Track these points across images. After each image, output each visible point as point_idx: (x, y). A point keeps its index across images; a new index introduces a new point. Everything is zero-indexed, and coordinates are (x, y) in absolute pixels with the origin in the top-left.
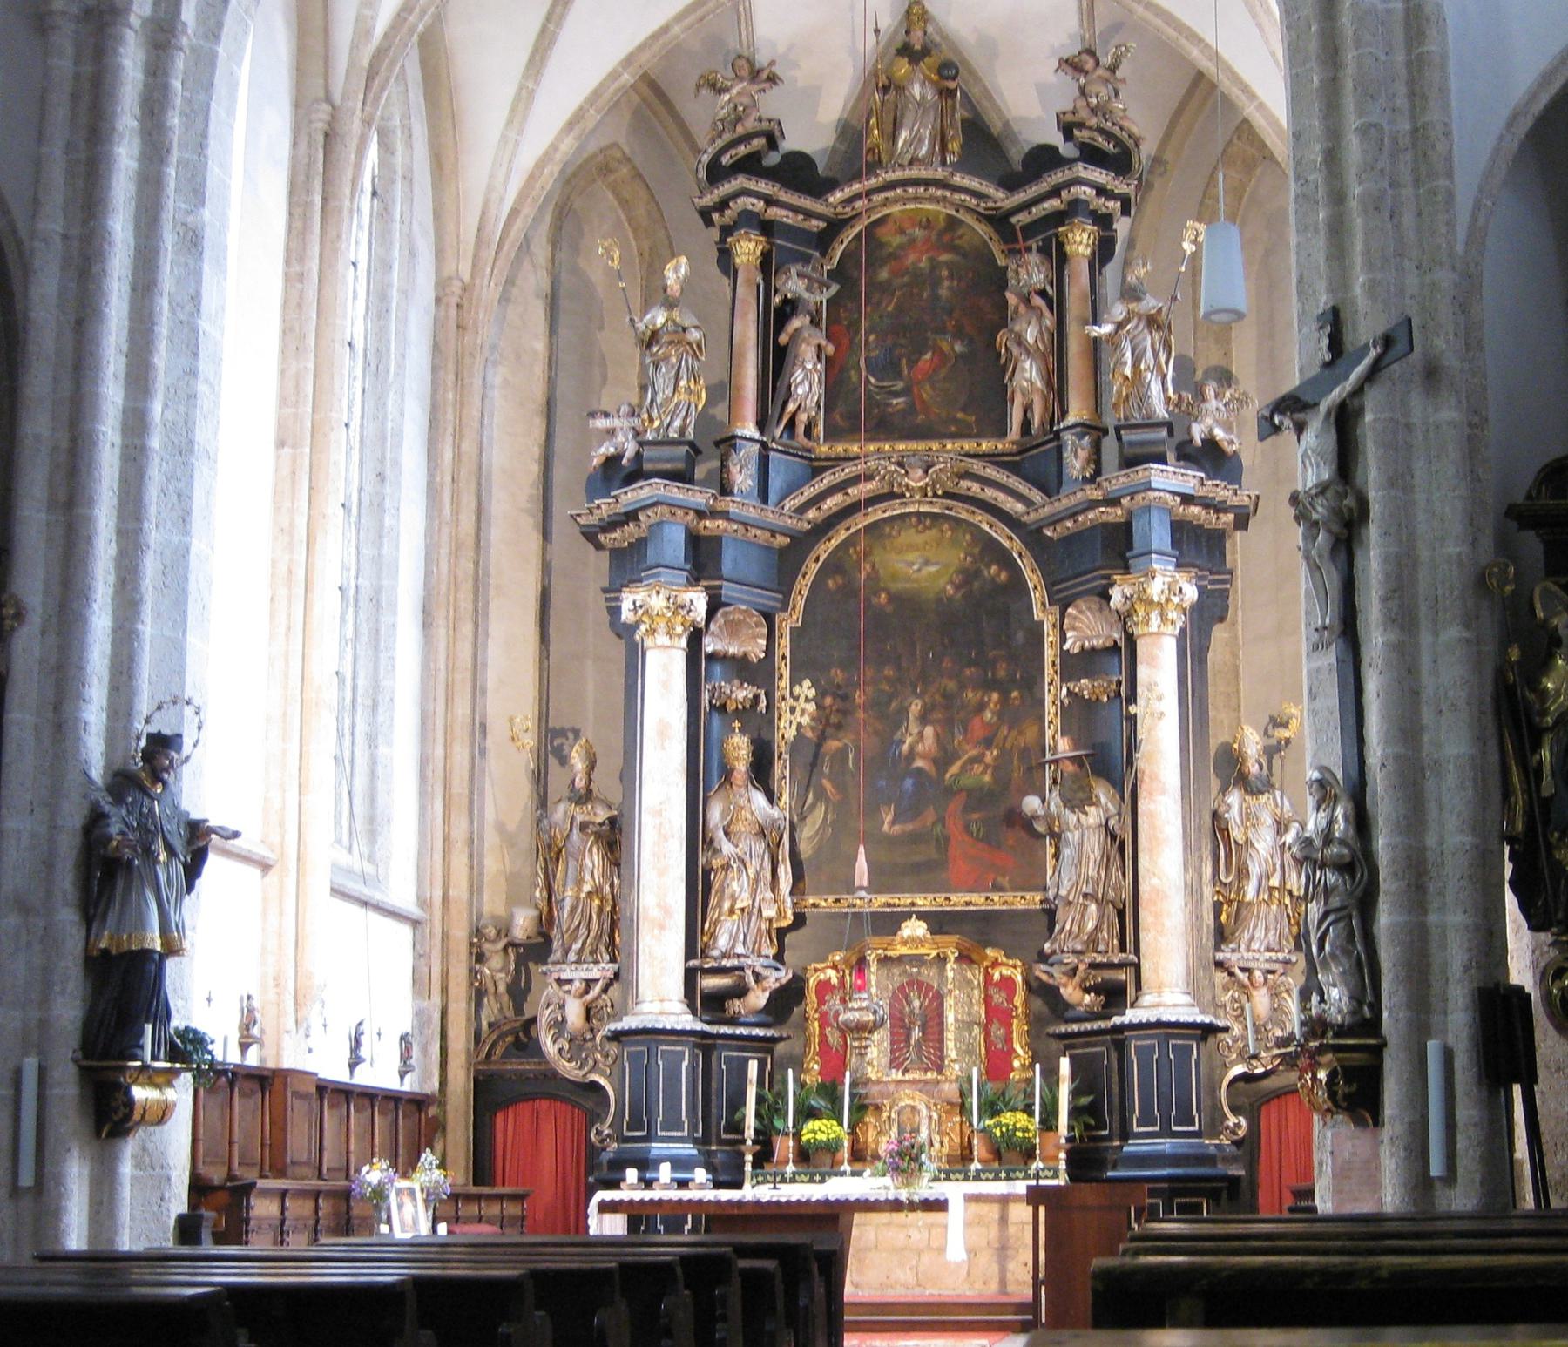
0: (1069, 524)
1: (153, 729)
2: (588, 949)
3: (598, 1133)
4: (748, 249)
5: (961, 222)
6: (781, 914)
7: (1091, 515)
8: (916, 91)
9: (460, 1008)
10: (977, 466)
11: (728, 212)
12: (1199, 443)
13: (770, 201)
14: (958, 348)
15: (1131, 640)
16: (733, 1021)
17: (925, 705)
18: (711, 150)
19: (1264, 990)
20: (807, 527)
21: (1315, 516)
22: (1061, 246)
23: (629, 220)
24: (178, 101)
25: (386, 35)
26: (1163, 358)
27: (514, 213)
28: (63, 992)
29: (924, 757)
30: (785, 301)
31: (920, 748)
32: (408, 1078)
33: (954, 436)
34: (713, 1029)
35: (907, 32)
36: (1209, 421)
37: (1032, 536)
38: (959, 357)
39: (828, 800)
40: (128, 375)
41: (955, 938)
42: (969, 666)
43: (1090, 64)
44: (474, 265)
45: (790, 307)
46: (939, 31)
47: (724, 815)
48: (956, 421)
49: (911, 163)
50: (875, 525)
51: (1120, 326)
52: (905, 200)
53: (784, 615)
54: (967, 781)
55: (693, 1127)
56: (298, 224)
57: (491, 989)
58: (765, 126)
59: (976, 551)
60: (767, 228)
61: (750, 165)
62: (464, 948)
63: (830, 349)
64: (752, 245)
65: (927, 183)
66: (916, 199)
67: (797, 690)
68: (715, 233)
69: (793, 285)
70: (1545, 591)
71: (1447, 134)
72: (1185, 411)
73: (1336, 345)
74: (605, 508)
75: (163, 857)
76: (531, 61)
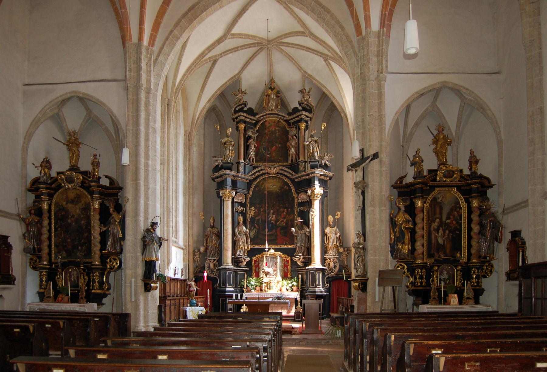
0: (300, 179)
2: (214, 254)
3: (216, 286)
4: (242, 126)
6: (248, 248)
7: (304, 177)
8: (272, 96)
11: (238, 119)
12: (324, 164)
13: (246, 117)
14: (280, 146)
15: (311, 201)
16: (240, 267)
17: (273, 212)
19: (333, 262)
21: (359, 187)
22: (299, 127)
24: (151, 104)
26: (317, 148)
27: (198, 118)
29: (273, 220)
30: (248, 136)
31: (272, 219)
33: (279, 162)
34: (236, 268)
35: (271, 85)
37: (293, 181)
44: (191, 128)
47: (238, 230)
48: (279, 159)
50: (264, 179)
51: (310, 142)
53: (248, 195)
54: (281, 225)
55: (233, 286)
58: (244, 102)
59: (283, 183)
60: (245, 122)
61: (241, 110)
63: (257, 145)
64: (242, 126)
65: (274, 114)
67: (251, 208)
68: (235, 123)
69: (250, 134)
72: (322, 158)
73: (363, 155)
74: (216, 175)
75: (155, 244)
76: (201, 89)
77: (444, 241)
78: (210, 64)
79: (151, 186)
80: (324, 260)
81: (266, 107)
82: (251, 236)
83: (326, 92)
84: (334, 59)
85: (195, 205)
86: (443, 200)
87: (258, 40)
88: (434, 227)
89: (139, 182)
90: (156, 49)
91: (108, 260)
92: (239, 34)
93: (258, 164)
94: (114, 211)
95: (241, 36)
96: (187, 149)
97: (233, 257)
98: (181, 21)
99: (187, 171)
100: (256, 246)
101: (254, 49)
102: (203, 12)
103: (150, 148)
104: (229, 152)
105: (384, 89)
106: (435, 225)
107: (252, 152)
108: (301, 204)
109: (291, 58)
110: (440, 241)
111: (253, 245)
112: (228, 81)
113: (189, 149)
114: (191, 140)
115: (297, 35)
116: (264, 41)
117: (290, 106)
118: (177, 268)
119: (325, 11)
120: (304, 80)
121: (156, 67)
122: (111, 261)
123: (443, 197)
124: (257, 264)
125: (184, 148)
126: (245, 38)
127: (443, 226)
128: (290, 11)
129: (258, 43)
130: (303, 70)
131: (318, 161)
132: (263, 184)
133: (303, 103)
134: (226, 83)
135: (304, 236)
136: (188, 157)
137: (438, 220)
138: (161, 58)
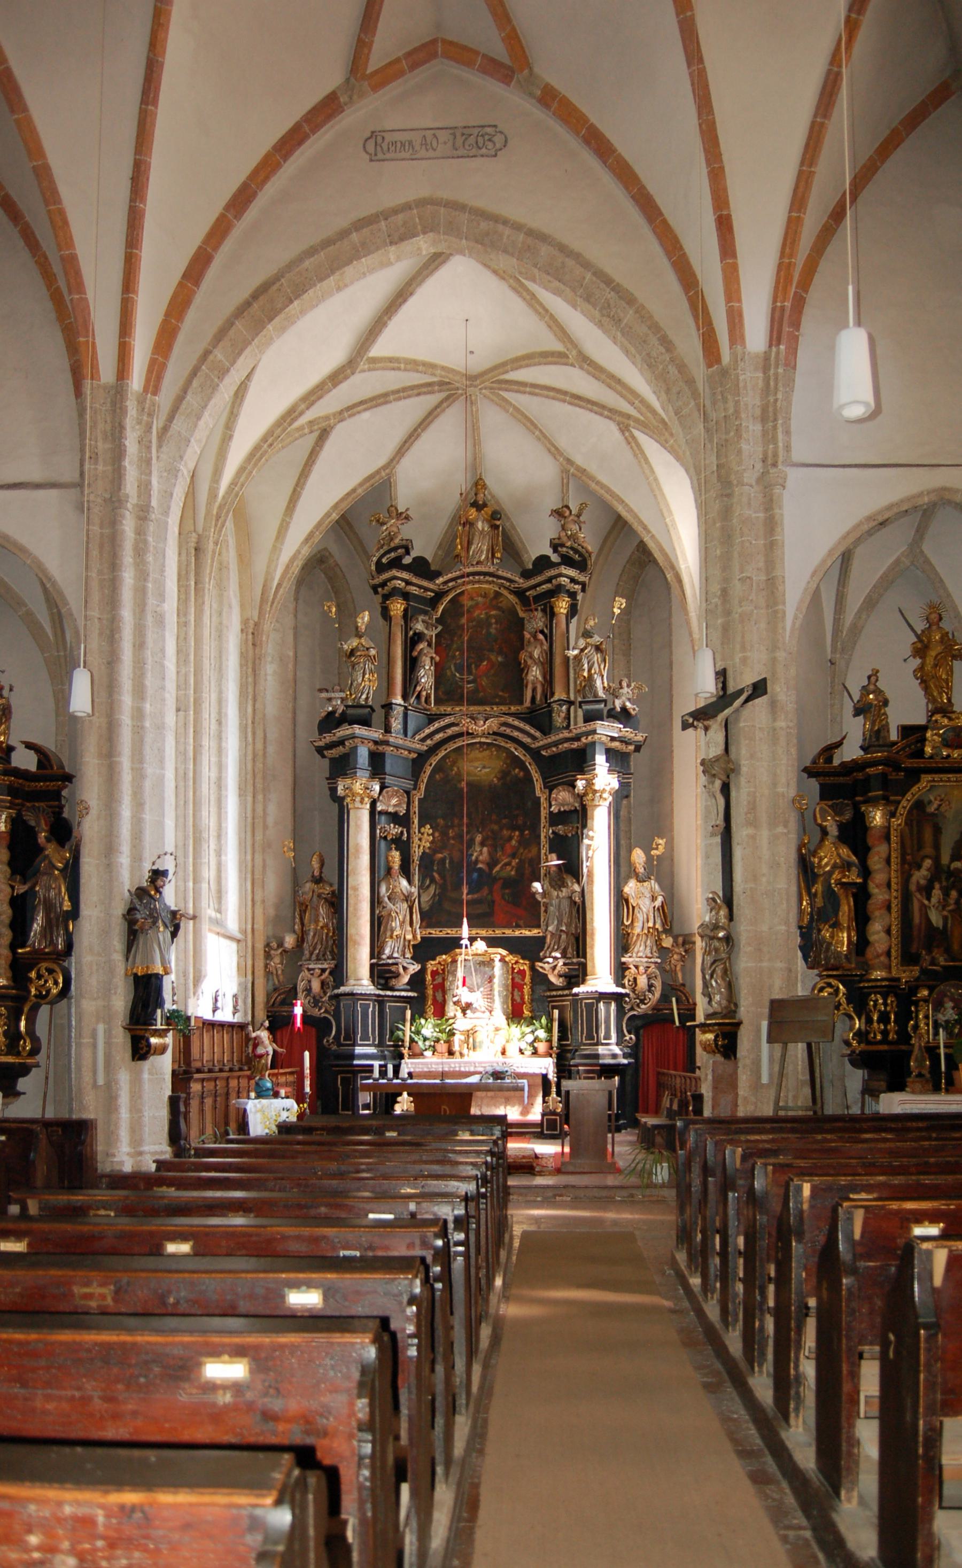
0: (554, 749)
1: (155, 868)
3: (328, 1041)
4: (397, 607)
5: (502, 594)
9: (260, 982)
10: (510, 720)
12: (619, 709)
13: (408, 583)
14: (500, 659)
18: (378, 555)
19: (645, 976)
20: (426, 748)
21: (714, 772)
22: (552, 608)
23: (332, 588)
25: (224, 497)
26: (602, 667)
28: (115, 993)
29: (482, 862)
30: (415, 634)
32: (236, 1015)
33: (497, 704)
35: (476, 494)
36: (624, 698)
37: (535, 754)
38: (501, 663)
39: (436, 883)
40: (134, 690)
41: (501, 951)
42: (505, 818)
43: (567, 513)
45: (418, 637)
46: (490, 493)
47: (388, 890)
49: (478, 563)
51: (582, 650)
52: (473, 583)
53: (414, 792)
54: (503, 874)
56: (183, 597)
57: (275, 972)
58: (404, 542)
59: (508, 762)
60: (406, 596)
61: (396, 563)
62: (262, 952)
63: (438, 659)
64: (399, 606)
65: (485, 574)
66: (479, 582)
67: (423, 830)
68: (378, 598)
69: (419, 627)
70: (821, 809)
71: (784, 582)
72: (613, 693)
73: (724, 688)
74: (328, 738)
75: (161, 929)
77: (945, 919)
78: (311, 439)
79: (150, 770)
80: (620, 970)
81: (463, 554)
82: (423, 905)
83: (624, 514)
84: (644, 426)
85: (270, 820)
86: (942, 809)
87: (441, 376)
88: (918, 882)
89: (117, 759)
90: (165, 399)
91: (33, 975)
92: (391, 360)
93: (442, 709)
94: (48, 840)
95: (396, 365)
96: (250, 670)
97: (374, 961)
98: (232, 324)
99: (249, 730)
100: (436, 933)
101: (431, 400)
102: (291, 302)
103: (148, 667)
104: (363, 677)
105: (781, 508)
106: (920, 876)
107: (426, 678)
108: (557, 818)
109: (529, 424)
110: (936, 919)
111: (429, 930)
112: (361, 485)
113: (254, 670)
114: (261, 644)
115: (544, 360)
116: (457, 378)
117: (527, 552)
118: (220, 993)
119: (620, 298)
120: (565, 481)
121: (164, 449)
122: (39, 977)
123: (941, 800)
124: (439, 980)
125: (241, 666)
126: (405, 370)
127: (943, 880)
128: (528, 297)
129: (441, 383)
130: (561, 454)
131: (605, 701)
132: (454, 763)
133: (563, 545)
134: (354, 490)
135: (565, 904)
136: (250, 690)
137: (928, 863)
138: (178, 425)
